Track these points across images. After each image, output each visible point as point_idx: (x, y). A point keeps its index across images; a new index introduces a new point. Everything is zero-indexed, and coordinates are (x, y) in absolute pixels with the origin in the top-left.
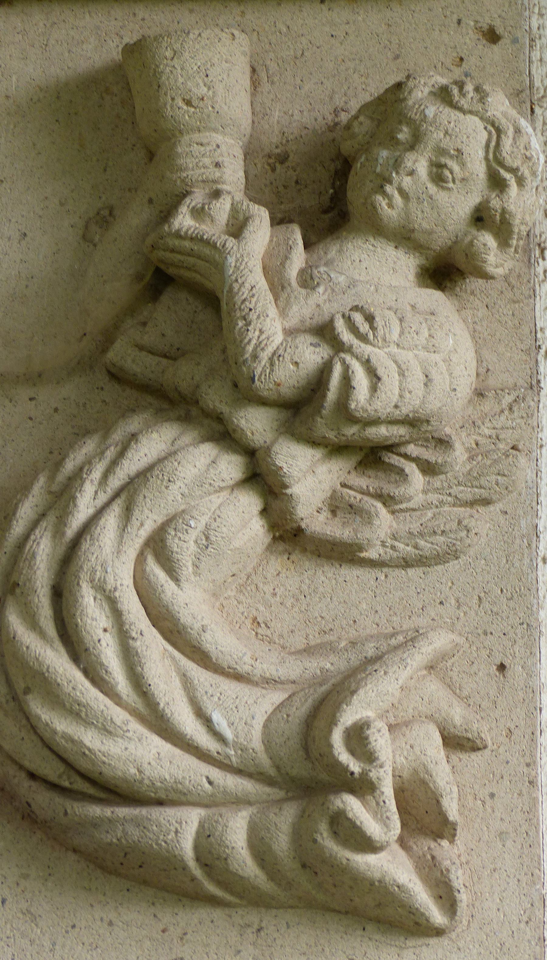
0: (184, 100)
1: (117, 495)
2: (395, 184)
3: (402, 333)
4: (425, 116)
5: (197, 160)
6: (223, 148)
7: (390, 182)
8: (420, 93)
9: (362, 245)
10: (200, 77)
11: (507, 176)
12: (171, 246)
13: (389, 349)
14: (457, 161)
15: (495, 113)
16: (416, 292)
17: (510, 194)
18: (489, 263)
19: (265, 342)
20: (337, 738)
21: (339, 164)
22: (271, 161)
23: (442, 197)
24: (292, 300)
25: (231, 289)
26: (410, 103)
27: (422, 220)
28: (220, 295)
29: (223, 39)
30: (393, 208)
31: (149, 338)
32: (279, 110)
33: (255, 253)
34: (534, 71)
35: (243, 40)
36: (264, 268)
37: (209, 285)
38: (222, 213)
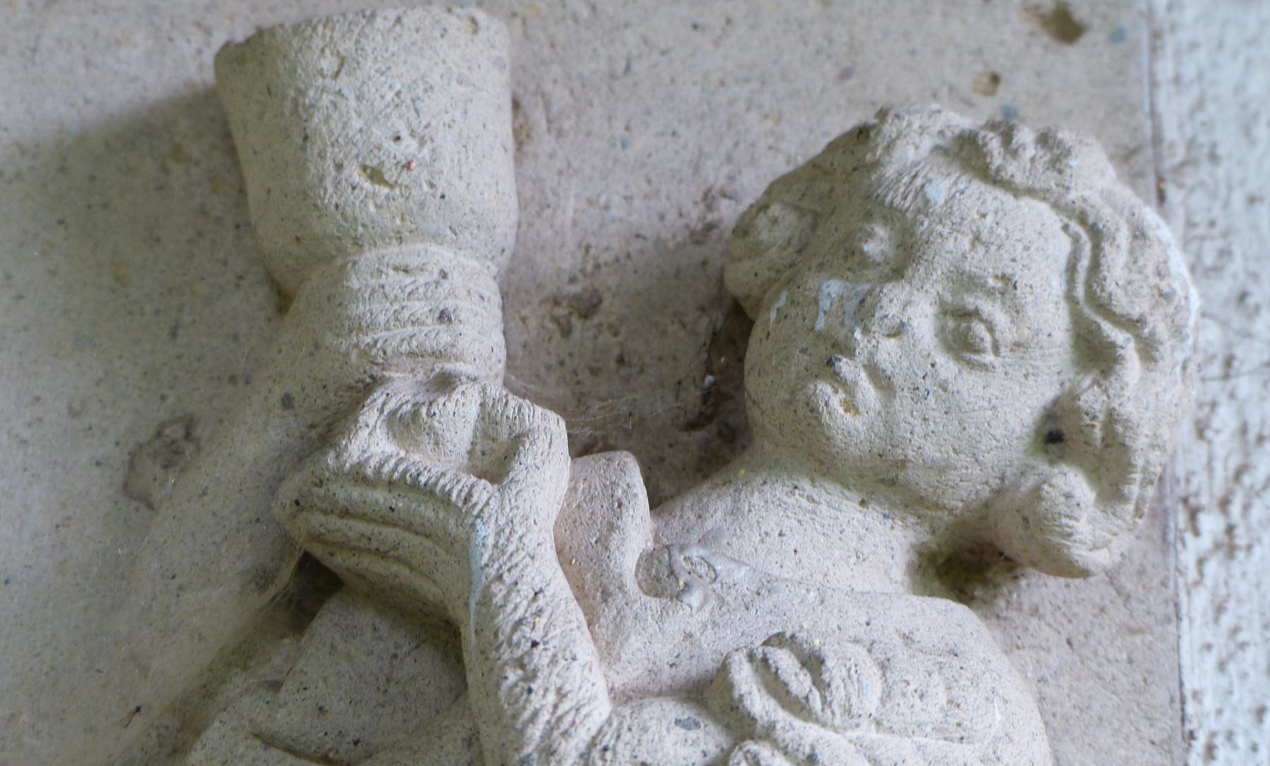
0: (365, 168)
2: (862, 358)
3: (887, 696)
4: (927, 201)
5: (396, 306)
6: (456, 278)
7: (850, 352)
8: (911, 151)
9: (785, 498)
10: (400, 117)
11: (1118, 336)
12: (342, 503)
13: (858, 733)
14: (1003, 303)
15: (1087, 193)
16: (914, 606)
17: (1126, 379)
18: (1077, 537)
19: (569, 718)
21: (718, 317)
22: (560, 312)
23: (968, 384)
24: (629, 622)
25: (487, 598)
26: (890, 172)
27: (924, 439)
28: (457, 613)
29: (452, 31)
30: (857, 412)
32: (577, 196)
34: (1162, 106)
35: (496, 33)
36: (559, 552)
37: (430, 590)
38: (460, 425)
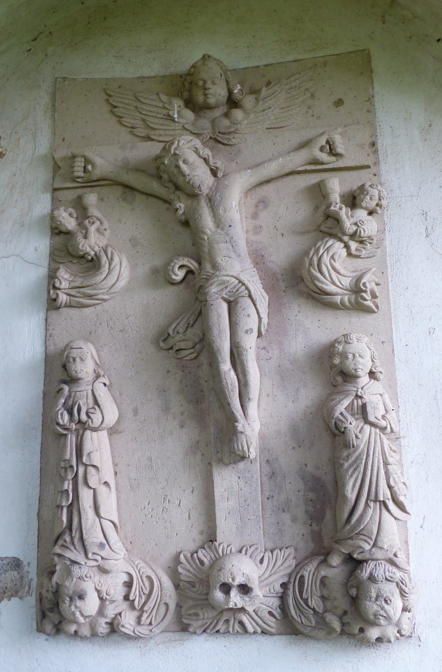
1: (326, 250)
8: (367, 186)
20: (361, 285)
23: (371, 202)
27: (369, 206)
31: (327, 226)
33: (344, 213)
